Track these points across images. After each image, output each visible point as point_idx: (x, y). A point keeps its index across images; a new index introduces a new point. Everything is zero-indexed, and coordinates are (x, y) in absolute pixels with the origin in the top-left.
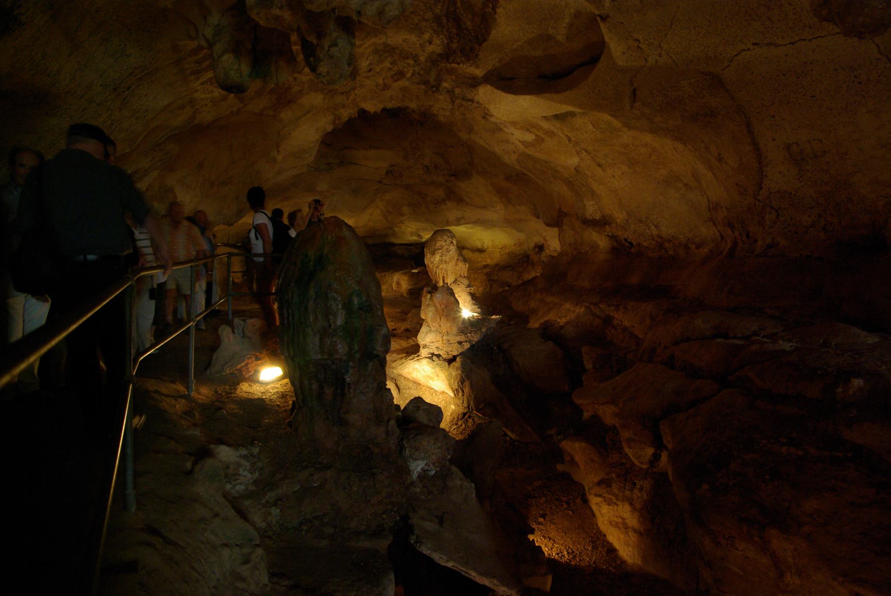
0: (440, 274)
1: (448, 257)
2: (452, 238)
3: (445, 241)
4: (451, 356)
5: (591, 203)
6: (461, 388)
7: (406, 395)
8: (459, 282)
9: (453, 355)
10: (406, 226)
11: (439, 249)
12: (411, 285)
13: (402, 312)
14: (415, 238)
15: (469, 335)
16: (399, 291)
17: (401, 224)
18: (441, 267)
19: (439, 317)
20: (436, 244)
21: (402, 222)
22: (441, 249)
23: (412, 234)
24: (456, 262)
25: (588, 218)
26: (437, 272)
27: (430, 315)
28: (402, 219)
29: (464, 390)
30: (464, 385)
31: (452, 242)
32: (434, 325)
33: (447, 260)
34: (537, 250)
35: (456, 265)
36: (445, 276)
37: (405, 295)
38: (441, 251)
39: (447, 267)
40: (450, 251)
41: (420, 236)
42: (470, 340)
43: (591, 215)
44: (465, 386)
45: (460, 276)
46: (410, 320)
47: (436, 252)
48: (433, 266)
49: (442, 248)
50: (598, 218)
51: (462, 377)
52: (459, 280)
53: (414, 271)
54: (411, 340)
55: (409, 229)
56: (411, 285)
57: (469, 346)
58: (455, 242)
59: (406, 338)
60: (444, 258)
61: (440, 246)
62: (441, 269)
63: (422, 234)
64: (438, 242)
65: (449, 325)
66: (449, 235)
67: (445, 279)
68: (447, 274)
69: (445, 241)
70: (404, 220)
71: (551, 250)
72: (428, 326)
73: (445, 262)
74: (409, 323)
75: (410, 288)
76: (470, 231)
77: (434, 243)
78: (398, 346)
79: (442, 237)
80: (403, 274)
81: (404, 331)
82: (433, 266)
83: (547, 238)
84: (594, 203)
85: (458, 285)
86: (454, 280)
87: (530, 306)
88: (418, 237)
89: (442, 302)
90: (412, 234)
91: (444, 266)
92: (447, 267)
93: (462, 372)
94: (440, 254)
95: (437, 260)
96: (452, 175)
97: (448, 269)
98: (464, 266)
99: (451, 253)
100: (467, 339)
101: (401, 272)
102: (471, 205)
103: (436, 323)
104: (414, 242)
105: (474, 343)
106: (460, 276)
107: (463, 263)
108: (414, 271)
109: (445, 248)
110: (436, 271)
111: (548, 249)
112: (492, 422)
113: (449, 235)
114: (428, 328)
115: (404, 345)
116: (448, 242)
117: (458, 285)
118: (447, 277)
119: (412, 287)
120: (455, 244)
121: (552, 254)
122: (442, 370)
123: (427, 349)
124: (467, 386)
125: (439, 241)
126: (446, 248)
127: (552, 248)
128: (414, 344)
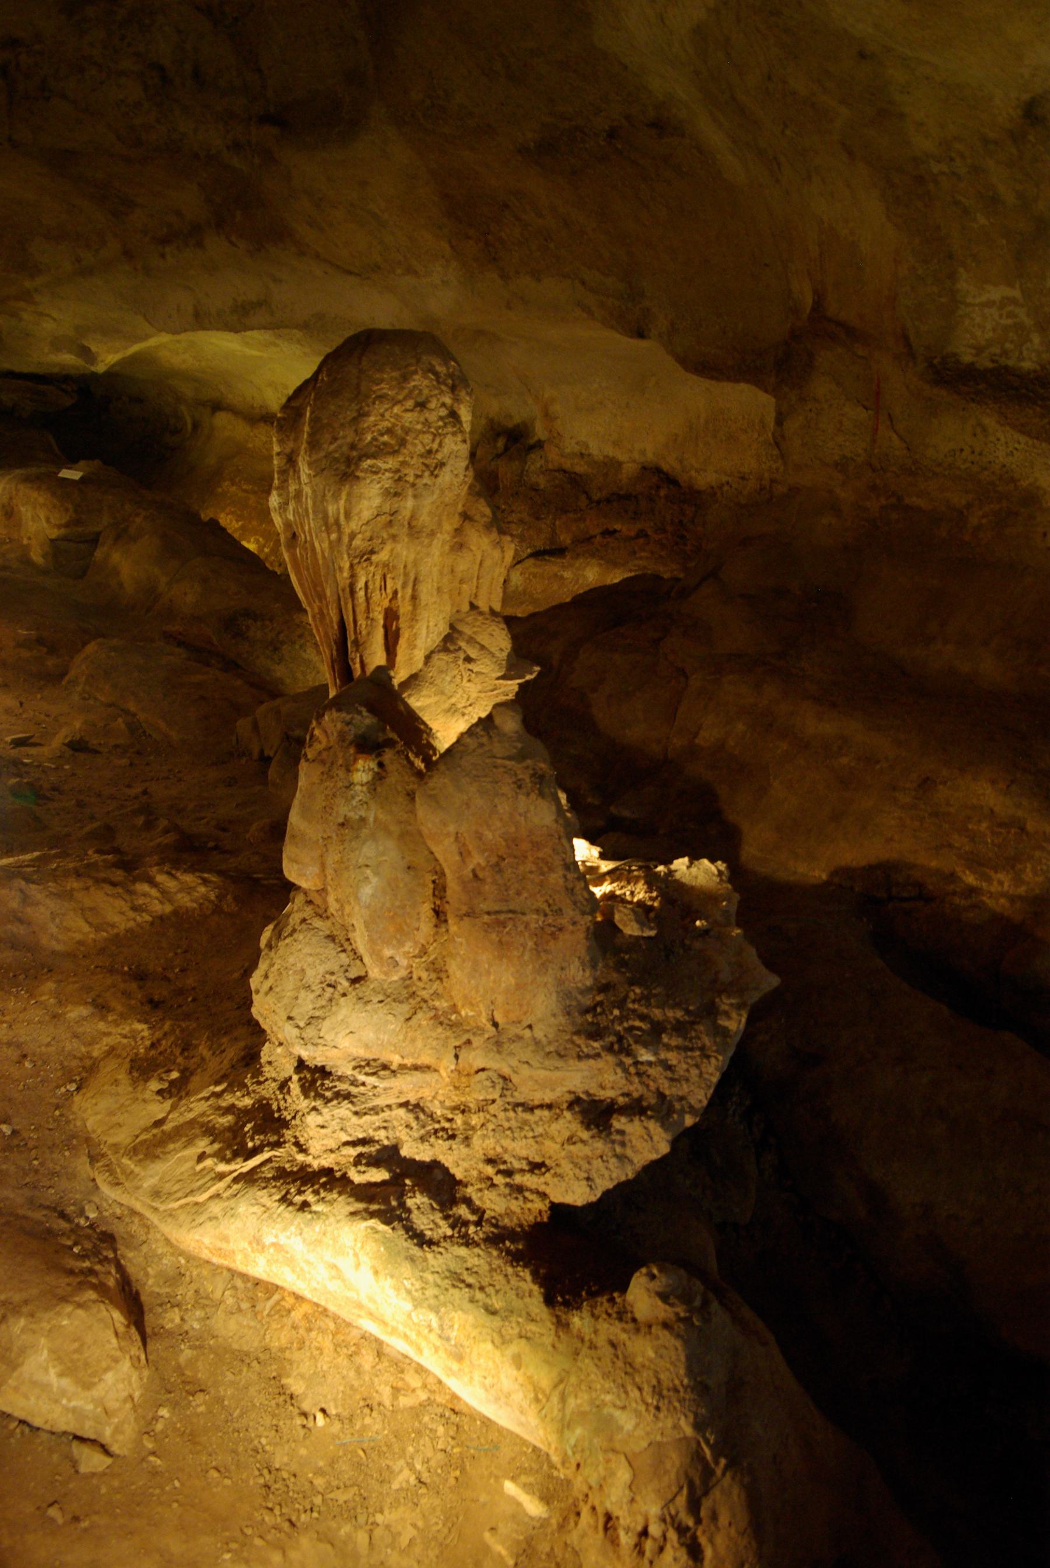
0: (376, 597)
1: (428, 502)
2: (453, 389)
3: (422, 405)
4: (539, 1205)
5: (996, 293)
6: (681, 1530)
7: (186, 1353)
8: (471, 640)
9: (558, 1197)
10: (41, 314)
11: (380, 451)
12: (67, 526)
13: (40, 641)
14: (68, 359)
15: (645, 1056)
16: (11, 540)
17: (22, 304)
18: (383, 556)
19: (426, 909)
20: (362, 415)
21: (26, 296)
22: (395, 453)
23: (57, 344)
24: (458, 531)
25: (967, 358)
26: (361, 584)
27: (367, 891)
28: (28, 284)
29: (703, 1540)
30: (703, 1513)
31: (453, 415)
32: (388, 952)
33: (424, 518)
34: (501, 443)
35: (459, 546)
36: (404, 608)
37: (37, 556)
38: (391, 463)
39: (416, 563)
40: (442, 465)
41: (85, 353)
42: (661, 1096)
43: (979, 350)
44: (714, 1517)
45: (473, 607)
46: (79, 689)
47: (367, 463)
48: (334, 546)
49: (403, 443)
50: (1027, 365)
51: (698, 1456)
52: (467, 630)
53: (66, 474)
54: (145, 887)
55: (48, 325)
56: (59, 527)
57: (664, 1149)
58: (465, 414)
59: (119, 875)
60: (410, 503)
61: (389, 431)
62: (387, 567)
63: (94, 349)
64: (380, 407)
65: (506, 976)
66: (441, 369)
67: (403, 623)
68: (414, 598)
69: (422, 405)
70: (36, 290)
71: (568, 451)
72: (331, 938)
73: (414, 530)
74: (76, 698)
75: (54, 533)
76: (254, 353)
77: (351, 414)
78: (86, 928)
79: (405, 378)
80: (27, 480)
81: (69, 752)
82: (334, 546)
83: (557, 408)
84: (1016, 293)
85: (468, 659)
86: (443, 629)
87: (696, 735)
88: (78, 355)
89: (480, 837)
90: (57, 344)
91: (404, 551)
92: (416, 563)
93: (699, 1426)
94: (386, 481)
95: (366, 515)
96: (266, 119)
97: (424, 569)
98: (496, 554)
99: (446, 477)
100: (636, 1089)
101: (18, 472)
102: (317, 256)
103: (408, 947)
104: (56, 370)
105: (689, 1121)
106: (473, 607)
107: (494, 535)
108: (66, 474)
109: (418, 445)
110: (353, 576)
111: (557, 446)
112: (591, 1342)
113: (441, 369)
114: (334, 960)
115: (117, 919)
116: (435, 413)
117: (468, 659)
118: (414, 618)
119: (63, 531)
120: (467, 427)
121: (567, 465)
122: (504, 1341)
123: (344, 1110)
124: (724, 1519)
125: (381, 397)
126: (420, 449)
127: (570, 446)
128: (168, 908)
